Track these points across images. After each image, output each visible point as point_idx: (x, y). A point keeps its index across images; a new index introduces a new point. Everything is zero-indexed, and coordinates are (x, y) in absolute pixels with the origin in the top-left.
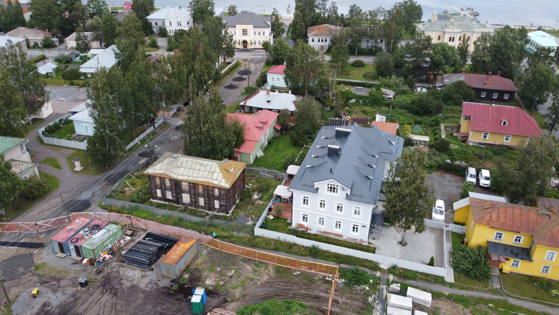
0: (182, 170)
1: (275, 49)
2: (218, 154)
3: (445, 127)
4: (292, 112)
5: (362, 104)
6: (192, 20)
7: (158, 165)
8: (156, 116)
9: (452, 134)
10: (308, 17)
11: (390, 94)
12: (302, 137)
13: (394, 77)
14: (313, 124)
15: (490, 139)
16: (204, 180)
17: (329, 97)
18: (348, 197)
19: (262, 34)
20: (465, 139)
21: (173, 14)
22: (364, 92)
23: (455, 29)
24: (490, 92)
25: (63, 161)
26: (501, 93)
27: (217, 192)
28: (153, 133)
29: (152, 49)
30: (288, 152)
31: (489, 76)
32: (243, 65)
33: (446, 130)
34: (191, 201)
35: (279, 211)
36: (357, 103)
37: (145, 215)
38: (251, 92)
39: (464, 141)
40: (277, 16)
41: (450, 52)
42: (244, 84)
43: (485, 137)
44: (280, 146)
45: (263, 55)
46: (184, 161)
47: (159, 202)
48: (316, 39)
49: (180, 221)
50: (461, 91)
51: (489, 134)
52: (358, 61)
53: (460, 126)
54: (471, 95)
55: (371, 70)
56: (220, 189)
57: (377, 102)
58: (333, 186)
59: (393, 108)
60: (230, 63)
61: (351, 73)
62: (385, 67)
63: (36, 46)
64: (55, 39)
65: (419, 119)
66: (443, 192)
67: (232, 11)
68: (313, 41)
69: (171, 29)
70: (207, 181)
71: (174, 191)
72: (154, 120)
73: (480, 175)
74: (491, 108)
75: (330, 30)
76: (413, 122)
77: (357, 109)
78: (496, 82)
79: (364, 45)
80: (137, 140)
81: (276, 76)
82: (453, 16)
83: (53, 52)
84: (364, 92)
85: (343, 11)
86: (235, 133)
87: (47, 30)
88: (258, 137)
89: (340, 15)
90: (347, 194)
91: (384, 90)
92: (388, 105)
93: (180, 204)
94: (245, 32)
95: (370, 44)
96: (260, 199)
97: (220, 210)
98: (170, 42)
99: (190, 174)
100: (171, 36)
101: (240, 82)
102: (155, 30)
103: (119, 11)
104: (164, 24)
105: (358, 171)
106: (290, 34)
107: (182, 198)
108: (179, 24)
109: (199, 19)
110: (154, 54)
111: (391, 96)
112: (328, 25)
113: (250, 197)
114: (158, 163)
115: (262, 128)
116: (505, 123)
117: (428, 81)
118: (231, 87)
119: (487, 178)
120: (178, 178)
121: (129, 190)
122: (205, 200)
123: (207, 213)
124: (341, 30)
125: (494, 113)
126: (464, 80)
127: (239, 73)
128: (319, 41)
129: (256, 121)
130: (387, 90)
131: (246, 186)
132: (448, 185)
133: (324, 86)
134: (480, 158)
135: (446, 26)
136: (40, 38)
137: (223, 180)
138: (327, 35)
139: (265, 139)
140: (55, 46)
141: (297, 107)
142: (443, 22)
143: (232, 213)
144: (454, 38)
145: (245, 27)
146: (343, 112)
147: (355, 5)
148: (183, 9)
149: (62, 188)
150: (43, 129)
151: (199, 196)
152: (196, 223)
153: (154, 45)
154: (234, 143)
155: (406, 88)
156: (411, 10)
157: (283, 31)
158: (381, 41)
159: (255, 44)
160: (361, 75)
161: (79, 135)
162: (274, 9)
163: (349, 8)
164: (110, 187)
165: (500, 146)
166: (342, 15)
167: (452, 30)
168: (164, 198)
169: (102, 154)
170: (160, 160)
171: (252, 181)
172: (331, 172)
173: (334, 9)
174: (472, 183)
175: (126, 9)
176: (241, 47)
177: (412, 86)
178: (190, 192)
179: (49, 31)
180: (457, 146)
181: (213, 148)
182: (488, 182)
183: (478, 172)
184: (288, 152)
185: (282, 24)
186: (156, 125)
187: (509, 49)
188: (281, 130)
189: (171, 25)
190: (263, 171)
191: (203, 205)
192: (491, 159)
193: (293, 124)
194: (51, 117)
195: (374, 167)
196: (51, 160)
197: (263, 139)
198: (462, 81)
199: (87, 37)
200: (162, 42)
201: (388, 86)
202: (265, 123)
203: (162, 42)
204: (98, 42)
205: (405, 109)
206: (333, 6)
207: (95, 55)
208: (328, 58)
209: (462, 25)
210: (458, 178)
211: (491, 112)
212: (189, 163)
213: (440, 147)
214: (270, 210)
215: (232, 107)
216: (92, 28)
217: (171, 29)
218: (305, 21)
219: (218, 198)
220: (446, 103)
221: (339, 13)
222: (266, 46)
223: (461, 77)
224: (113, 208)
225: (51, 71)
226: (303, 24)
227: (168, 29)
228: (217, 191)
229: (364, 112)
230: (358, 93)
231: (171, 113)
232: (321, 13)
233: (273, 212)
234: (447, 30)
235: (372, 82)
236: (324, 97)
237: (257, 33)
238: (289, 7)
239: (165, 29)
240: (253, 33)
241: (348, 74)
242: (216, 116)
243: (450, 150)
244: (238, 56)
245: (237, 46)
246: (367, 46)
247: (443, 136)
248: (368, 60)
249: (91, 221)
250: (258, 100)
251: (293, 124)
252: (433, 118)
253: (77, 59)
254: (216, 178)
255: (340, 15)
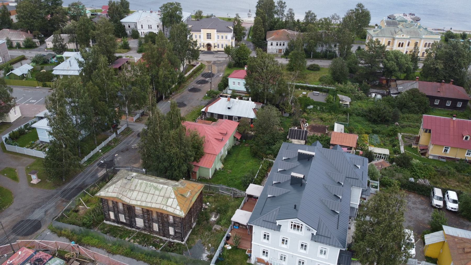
0: (135, 193)
1: (238, 52)
2: (175, 170)
3: (403, 137)
4: (252, 119)
5: (320, 110)
6: (162, 23)
7: (111, 187)
8: (118, 122)
9: (410, 146)
10: (268, 20)
11: (346, 100)
12: (261, 148)
13: (349, 83)
14: (273, 135)
15: (451, 153)
16: (158, 206)
17: (288, 103)
18: (314, 238)
19: (224, 37)
20: (424, 151)
21: (144, 20)
22: (320, 98)
23: (405, 35)
24: (443, 100)
25: (21, 172)
26: (455, 101)
27: (171, 219)
28: (116, 140)
29: (123, 50)
30: (247, 165)
31: (443, 84)
32: (207, 68)
33: (405, 142)
34: (145, 225)
35: (237, 240)
36: (315, 109)
37: (95, 241)
38: (213, 97)
39: (423, 154)
40: (239, 22)
41: (403, 60)
42: (206, 88)
43: (446, 151)
44: (240, 157)
45: (226, 58)
46: (138, 183)
47: (113, 224)
48: (275, 43)
49: (132, 250)
50: (415, 99)
51: (450, 148)
52: (314, 65)
53: (419, 138)
54: (425, 103)
55: (326, 74)
56: (175, 217)
57: (333, 108)
58: (297, 225)
59: (350, 115)
60: (195, 66)
61: (307, 76)
62: (341, 73)
63: (18, 46)
64: (36, 40)
65: (377, 128)
66: (410, 217)
67: (199, 16)
68: (272, 44)
69: (143, 31)
70: (161, 208)
71: (127, 214)
72: (117, 125)
73: (446, 196)
74: (452, 122)
75: (288, 35)
76: (371, 132)
77: (314, 116)
78: (449, 90)
79: (319, 49)
80: (98, 149)
81: (237, 81)
82: (400, 23)
83: (33, 52)
84: (320, 98)
85: (300, 17)
86: (194, 147)
87: (29, 32)
88: (217, 145)
89: (296, 21)
90: (313, 234)
91: (340, 96)
92: (345, 113)
93: (133, 227)
94: (209, 36)
95: (324, 49)
96: (218, 222)
97: (175, 237)
98: (140, 44)
99: (143, 199)
100: (142, 38)
101: (203, 85)
102: (128, 32)
103: (99, 13)
104: (136, 27)
105: (324, 204)
106: (250, 37)
107: (135, 222)
108: (150, 27)
109: (167, 22)
110: (125, 55)
111: (348, 103)
112: (286, 30)
113: (208, 219)
114: (112, 184)
115: (222, 140)
116: (467, 138)
117: (380, 86)
118: (194, 90)
119: (454, 202)
120: (130, 203)
121: (83, 209)
122: (159, 226)
123: (161, 239)
124: (299, 35)
125: (455, 127)
126: (418, 87)
127: (203, 75)
128: (277, 45)
129: (216, 133)
130: (343, 96)
131: (204, 205)
132: (413, 208)
133: (282, 92)
134: (443, 174)
135: (396, 33)
136: (22, 39)
137: (178, 208)
138: (286, 40)
139: (224, 150)
140: (36, 47)
141: (257, 116)
142: (392, 28)
143: (188, 240)
144: (403, 43)
145: (209, 31)
146: (302, 120)
147: (309, 12)
148: (153, 13)
149: (15, 205)
150: (7, 136)
151: (153, 222)
152: (149, 254)
153: (126, 47)
154: (193, 158)
155: (361, 94)
156: (362, 16)
157: (244, 34)
158: (335, 46)
159: (218, 47)
160: (317, 80)
161: (42, 142)
162: (237, 15)
163: (305, 15)
164: (64, 203)
165: (461, 160)
166: (298, 21)
167: (401, 37)
168: (117, 220)
169: (61, 166)
170: (115, 179)
171: (210, 199)
172: (295, 208)
173: (291, 14)
174: (440, 206)
175: (103, 12)
176: (205, 49)
177: (367, 92)
178: (143, 217)
179: (31, 33)
180: (418, 161)
181: (170, 165)
182: (456, 206)
183: (444, 192)
184: (247, 165)
185: (243, 29)
186: (118, 132)
187: (460, 57)
188: (241, 139)
189: (142, 28)
190: (222, 189)
191: (158, 230)
192: (454, 176)
193: (253, 133)
194: (18, 121)
195: (341, 197)
196: (11, 170)
197: (222, 150)
198: (416, 89)
199: (63, 39)
200: (133, 43)
201: (344, 92)
202: (225, 135)
203: (133, 43)
204: (75, 44)
205: (362, 116)
206: (291, 13)
207: (67, 58)
208: (284, 62)
209: (410, 32)
210: (423, 198)
211: (452, 126)
212: (144, 186)
213: (403, 162)
214: (228, 238)
215: (194, 112)
216: (69, 31)
217: (143, 31)
218: (264, 26)
219: (173, 225)
220: (401, 110)
221: (296, 19)
222: (228, 50)
223: (415, 85)
224: (63, 232)
225: (26, 72)
226: (263, 29)
227: (140, 32)
228: (171, 218)
229: (321, 119)
230: (316, 99)
231: (135, 119)
232: (279, 18)
233: (230, 241)
234: (397, 36)
235: (328, 87)
236: (283, 104)
237: (220, 37)
238: (250, 11)
239: (137, 32)
240: (216, 37)
241: (305, 78)
242: (172, 132)
243: (412, 166)
244: (203, 58)
245: (202, 49)
246: (322, 50)
247: (402, 150)
248: (325, 64)
249: (35, 253)
250: (219, 107)
251: (253, 133)
252: (390, 128)
253: (54, 60)
254: (170, 205)
255: (296, 21)
